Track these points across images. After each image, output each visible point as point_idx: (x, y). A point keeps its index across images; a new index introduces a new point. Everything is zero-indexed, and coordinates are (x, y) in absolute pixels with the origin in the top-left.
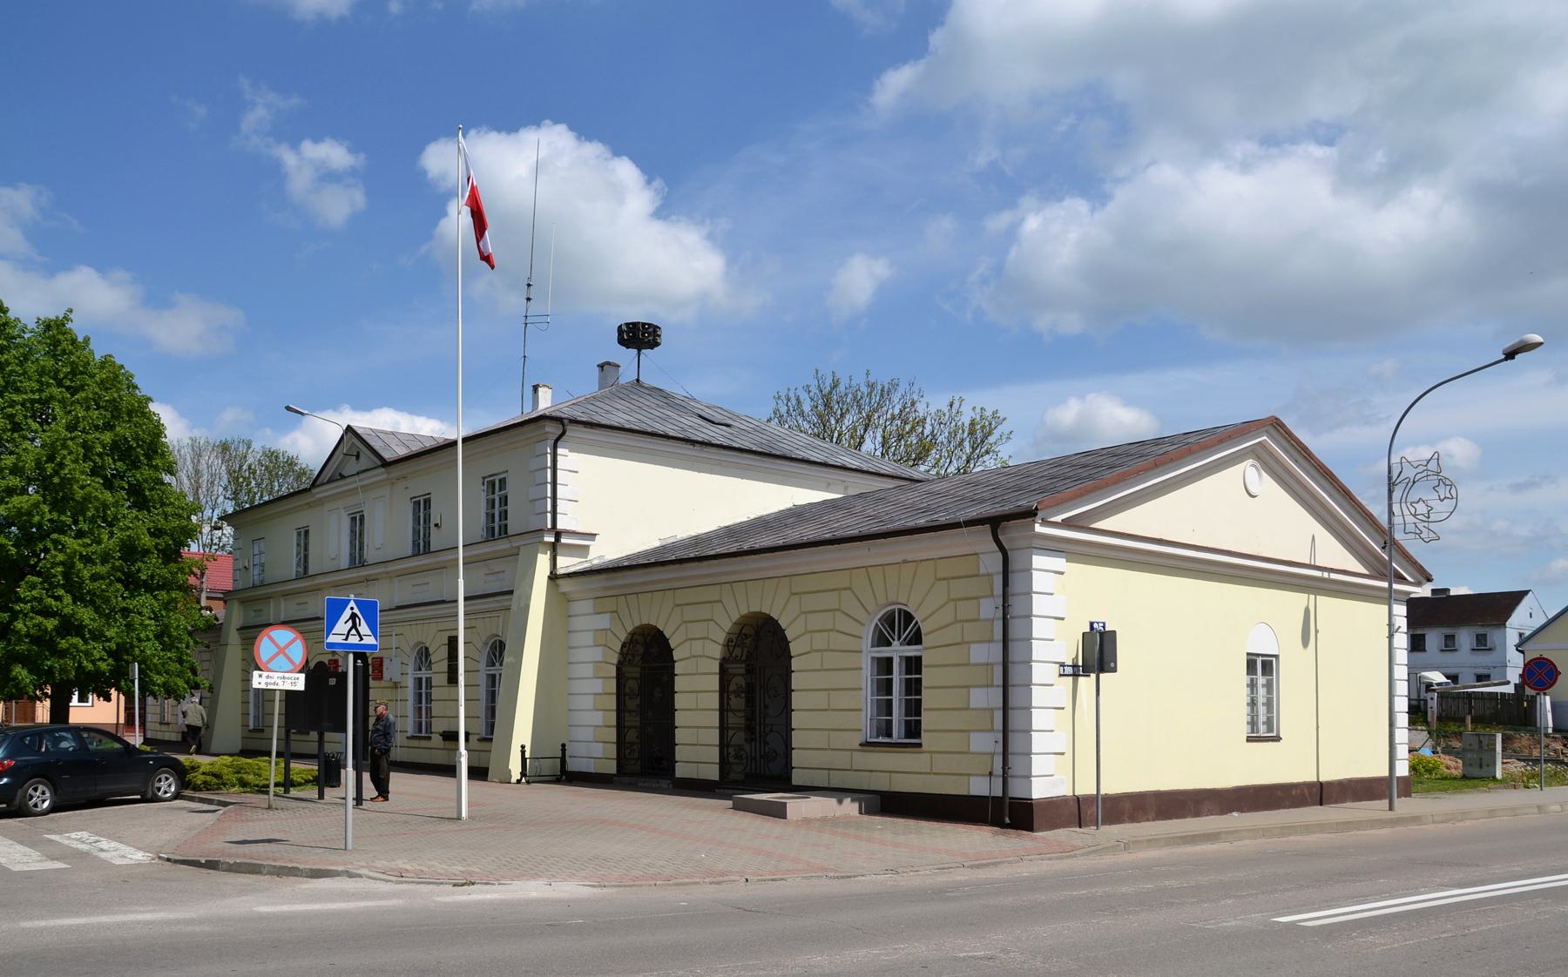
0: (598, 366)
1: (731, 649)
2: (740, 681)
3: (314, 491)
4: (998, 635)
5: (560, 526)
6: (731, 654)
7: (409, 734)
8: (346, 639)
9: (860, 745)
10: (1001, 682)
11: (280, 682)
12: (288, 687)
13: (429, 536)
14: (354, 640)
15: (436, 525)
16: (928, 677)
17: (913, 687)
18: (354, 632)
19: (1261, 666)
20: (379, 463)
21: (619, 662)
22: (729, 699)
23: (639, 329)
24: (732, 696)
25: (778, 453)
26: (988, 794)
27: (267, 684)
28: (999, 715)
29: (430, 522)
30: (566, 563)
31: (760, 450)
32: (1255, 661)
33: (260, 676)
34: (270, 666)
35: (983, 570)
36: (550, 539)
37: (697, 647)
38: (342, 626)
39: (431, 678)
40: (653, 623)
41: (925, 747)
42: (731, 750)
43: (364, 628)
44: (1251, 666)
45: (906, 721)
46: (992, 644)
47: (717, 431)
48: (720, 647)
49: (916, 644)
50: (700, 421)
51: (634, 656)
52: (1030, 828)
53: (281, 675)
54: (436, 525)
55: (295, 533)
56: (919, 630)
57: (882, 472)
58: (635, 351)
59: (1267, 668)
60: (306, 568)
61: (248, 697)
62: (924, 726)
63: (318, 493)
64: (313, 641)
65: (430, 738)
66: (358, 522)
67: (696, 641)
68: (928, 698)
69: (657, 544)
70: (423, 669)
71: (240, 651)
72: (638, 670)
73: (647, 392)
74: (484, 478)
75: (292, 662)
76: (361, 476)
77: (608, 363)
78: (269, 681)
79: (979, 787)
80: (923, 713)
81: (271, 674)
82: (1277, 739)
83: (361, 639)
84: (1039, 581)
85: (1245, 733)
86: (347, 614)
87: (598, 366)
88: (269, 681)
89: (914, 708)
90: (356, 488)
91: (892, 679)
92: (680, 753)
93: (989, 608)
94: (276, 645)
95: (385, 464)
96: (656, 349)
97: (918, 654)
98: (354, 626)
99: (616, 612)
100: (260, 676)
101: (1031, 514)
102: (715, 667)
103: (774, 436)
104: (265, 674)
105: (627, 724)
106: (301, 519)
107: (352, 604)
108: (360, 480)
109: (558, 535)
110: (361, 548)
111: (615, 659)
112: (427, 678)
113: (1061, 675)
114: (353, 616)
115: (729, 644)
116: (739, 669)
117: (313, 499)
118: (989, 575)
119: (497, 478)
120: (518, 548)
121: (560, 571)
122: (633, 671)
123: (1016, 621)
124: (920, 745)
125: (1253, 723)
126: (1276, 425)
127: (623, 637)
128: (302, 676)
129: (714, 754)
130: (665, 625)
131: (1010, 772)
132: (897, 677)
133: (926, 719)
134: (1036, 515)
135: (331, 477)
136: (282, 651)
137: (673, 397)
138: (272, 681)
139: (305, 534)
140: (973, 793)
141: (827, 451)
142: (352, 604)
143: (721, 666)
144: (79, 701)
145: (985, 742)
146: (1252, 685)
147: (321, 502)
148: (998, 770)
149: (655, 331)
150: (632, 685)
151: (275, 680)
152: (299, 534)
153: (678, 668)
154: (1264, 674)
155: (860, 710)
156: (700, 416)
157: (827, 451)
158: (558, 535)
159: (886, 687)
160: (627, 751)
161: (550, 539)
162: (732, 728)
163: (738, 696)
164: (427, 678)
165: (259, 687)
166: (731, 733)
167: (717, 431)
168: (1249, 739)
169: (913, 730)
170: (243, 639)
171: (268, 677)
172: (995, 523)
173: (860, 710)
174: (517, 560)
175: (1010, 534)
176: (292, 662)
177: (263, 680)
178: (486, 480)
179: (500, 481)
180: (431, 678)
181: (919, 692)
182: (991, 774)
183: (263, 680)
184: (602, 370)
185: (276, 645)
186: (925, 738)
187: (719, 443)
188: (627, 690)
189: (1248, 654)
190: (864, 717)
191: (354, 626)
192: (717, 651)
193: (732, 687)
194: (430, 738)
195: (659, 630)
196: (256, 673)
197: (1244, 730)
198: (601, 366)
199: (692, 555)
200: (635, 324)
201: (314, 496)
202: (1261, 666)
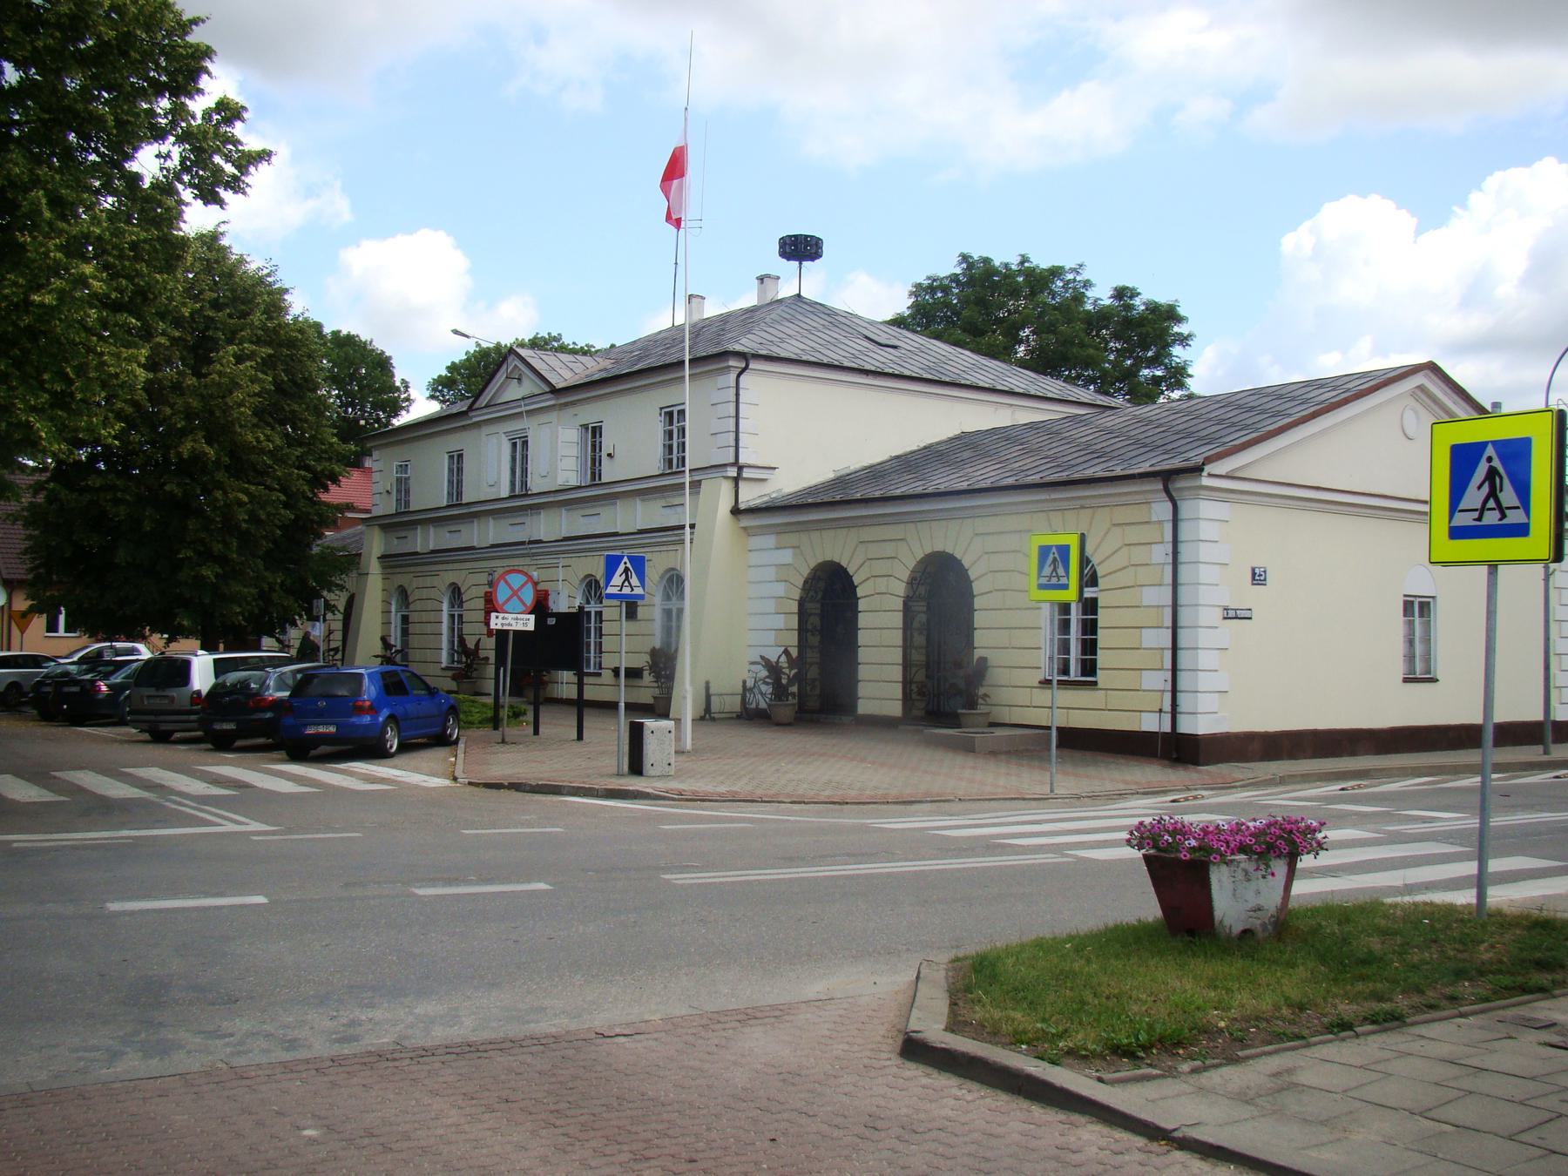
0: (757, 278)
1: (915, 586)
2: (922, 618)
3: (471, 414)
4: (1168, 579)
5: (742, 460)
6: (915, 593)
7: (443, 665)
8: (621, 590)
9: (1040, 682)
10: (1169, 624)
11: (513, 622)
12: (520, 627)
13: (600, 465)
14: (626, 591)
15: (609, 455)
16: (1103, 618)
17: (1090, 627)
18: (626, 584)
19: (1418, 608)
20: (547, 390)
21: (801, 598)
22: (912, 636)
23: (801, 243)
24: (916, 634)
25: (947, 380)
26: (1157, 730)
27: (502, 625)
28: (1168, 654)
29: (600, 450)
30: (750, 495)
31: (930, 377)
32: (1412, 602)
33: (497, 617)
34: (505, 607)
35: (1154, 519)
36: (733, 472)
37: (882, 584)
38: (617, 579)
39: (601, 612)
40: (836, 560)
41: (1100, 686)
42: (914, 687)
43: (634, 581)
44: (1408, 607)
45: (1082, 660)
46: (1162, 588)
47: (886, 355)
48: (904, 584)
49: (1092, 586)
50: (866, 344)
51: (816, 592)
52: (1197, 763)
53: (515, 616)
54: (609, 455)
55: (446, 456)
56: (1095, 572)
57: (1050, 395)
58: (796, 263)
59: (1425, 610)
60: (460, 494)
61: (390, 630)
62: (1099, 665)
63: (475, 416)
64: (467, 572)
65: (599, 675)
66: (520, 447)
67: (880, 579)
68: (1103, 637)
69: (831, 476)
70: (592, 602)
71: (380, 580)
72: (818, 606)
73: (810, 309)
74: (661, 409)
75: (524, 604)
76: (527, 401)
77: (768, 276)
78: (504, 622)
79: (1151, 723)
80: (1099, 652)
81: (506, 615)
82: (1434, 680)
83: (632, 590)
84: (1206, 530)
85: (1402, 673)
86: (621, 568)
87: (757, 278)
88: (504, 622)
89: (1090, 647)
90: (522, 413)
91: (1069, 619)
92: (863, 690)
93: (1162, 553)
94: (511, 588)
95: (555, 391)
96: (817, 261)
97: (1094, 595)
98: (627, 579)
99: (798, 547)
100: (497, 617)
101: (1198, 470)
102: (899, 603)
103: (939, 357)
104: (501, 615)
105: (808, 660)
106: (454, 442)
107: (625, 559)
108: (525, 405)
109: (740, 468)
110: (525, 471)
111: (797, 594)
112: (596, 612)
113: (1225, 618)
114: (626, 570)
115: (912, 582)
116: (920, 607)
117: (469, 422)
118: (1160, 522)
119: (675, 409)
120: (700, 481)
121: (742, 506)
122: (814, 607)
123: (1182, 716)
124: (1095, 683)
125: (1410, 658)
126: (1432, 368)
127: (806, 572)
128: (532, 617)
129: (897, 691)
130: (1096, 550)
131: (1179, 709)
132: (1075, 616)
133: (1102, 658)
134: (1202, 470)
135: (490, 401)
136: (515, 593)
137: (837, 314)
138: (507, 622)
139: (457, 459)
140: (1145, 728)
141: (992, 371)
142: (625, 559)
143: (905, 603)
144: (66, 632)
145: (1158, 680)
146: (1411, 624)
147: (478, 425)
148: (1167, 707)
149: (817, 244)
150: (815, 621)
151: (509, 621)
152: (451, 457)
153: (862, 605)
154: (1421, 615)
155: (1040, 648)
156: (867, 337)
157: (992, 371)
158: (740, 468)
159: (1065, 626)
160: (808, 688)
161: (733, 472)
162: (917, 665)
163: (921, 633)
164: (596, 612)
165: (497, 627)
166: (914, 670)
167: (886, 355)
168: (1406, 680)
169: (1089, 668)
170: (384, 568)
171: (503, 618)
172: (1167, 477)
173: (1040, 648)
174: (699, 493)
175: (1181, 483)
176: (524, 604)
177: (500, 621)
178: (663, 411)
179: (679, 411)
180: (601, 612)
181: (1094, 632)
182: (1161, 711)
183: (500, 621)
184: (762, 283)
185: (511, 588)
186: (1101, 677)
187: (891, 371)
188: (810, 627)
189: (1405, 596)
190: (1043, 656)
191: (627, 579)
192: (900, 588)
193: (916, 624)
194: (599, 675)
195: (842, 567)
196: (493, 615)
197: (1399, 669)
198: (761, 279)
199: (838, 498)
200: (796, 236)
201: (471, 418)
202: (1418, 608)
